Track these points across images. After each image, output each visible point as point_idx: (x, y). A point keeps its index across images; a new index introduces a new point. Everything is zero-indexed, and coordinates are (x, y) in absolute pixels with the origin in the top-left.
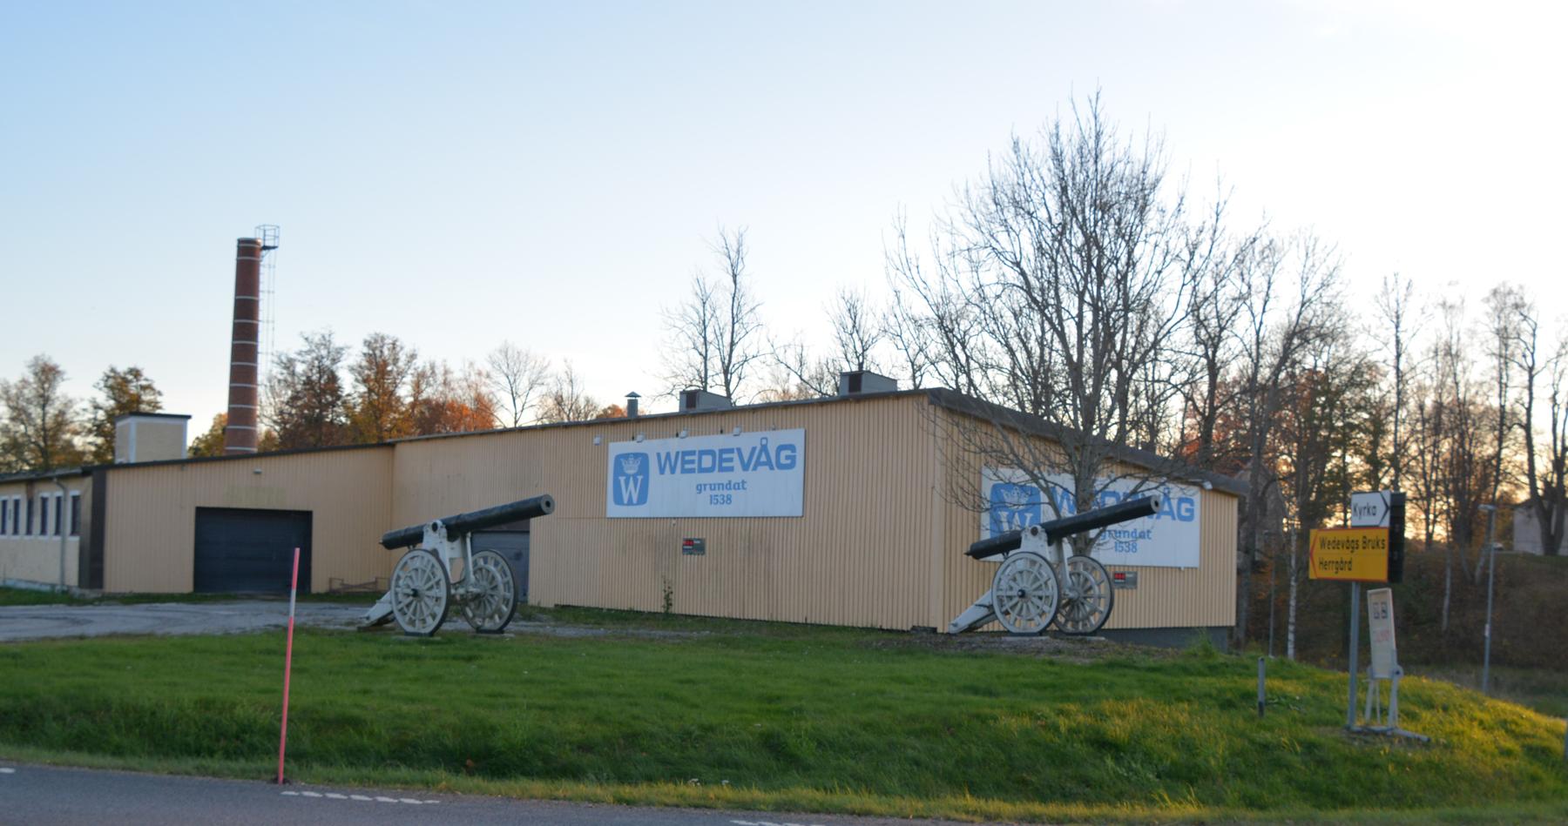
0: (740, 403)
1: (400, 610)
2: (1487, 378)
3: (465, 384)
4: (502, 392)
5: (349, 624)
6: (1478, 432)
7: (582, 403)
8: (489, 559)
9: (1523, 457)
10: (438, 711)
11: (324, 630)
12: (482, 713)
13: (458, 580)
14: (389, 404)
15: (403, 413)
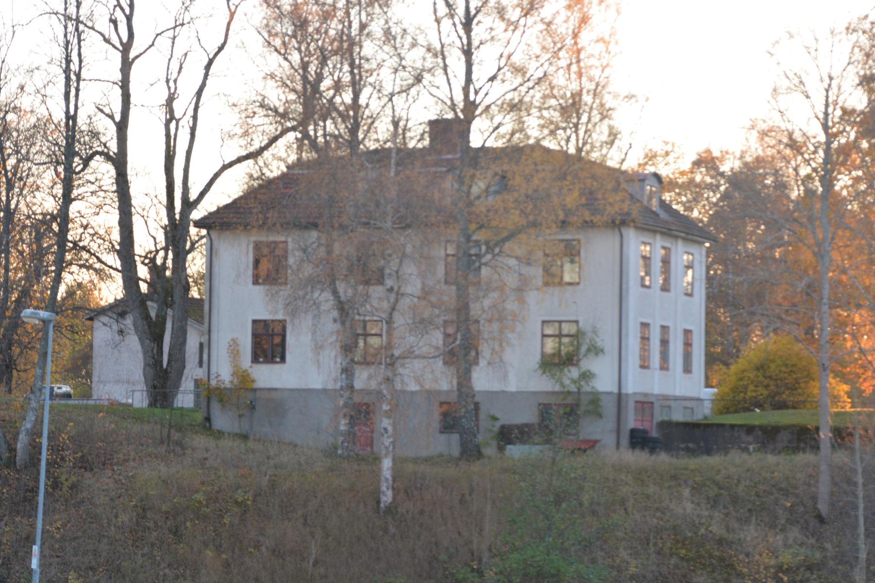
2: (42, 61)
6: (26, 165)
9: (111, 219)
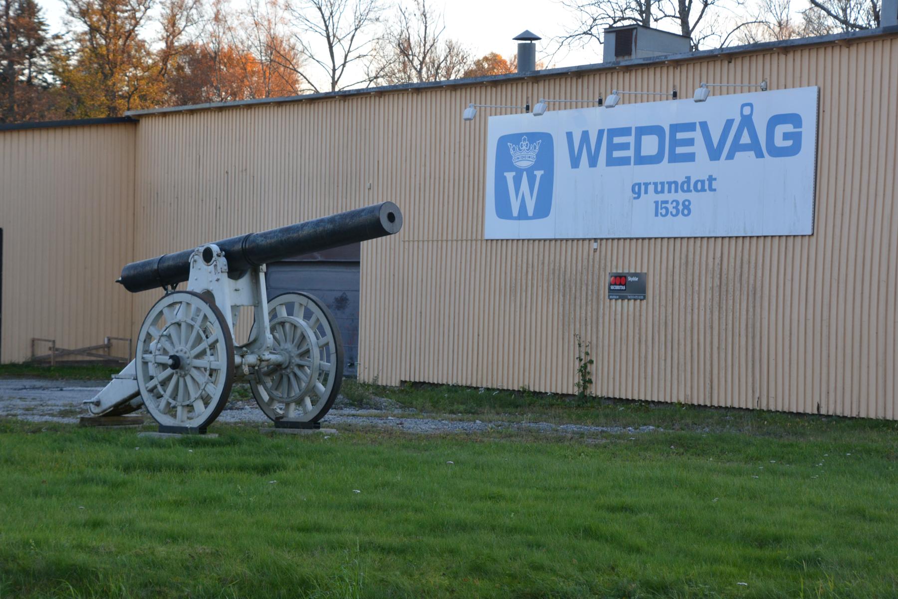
0: (705, 46)
1: (151, 391)
3: (249, 20)
4: (311, 33)
5: (64, 414)
7: (441, 51)
8: (296, 306)
10: (216, 554)
11: (23, 423)
12: (287, 558)
13: (245, 342)
14: (125, 50)
15: (148, 68)
